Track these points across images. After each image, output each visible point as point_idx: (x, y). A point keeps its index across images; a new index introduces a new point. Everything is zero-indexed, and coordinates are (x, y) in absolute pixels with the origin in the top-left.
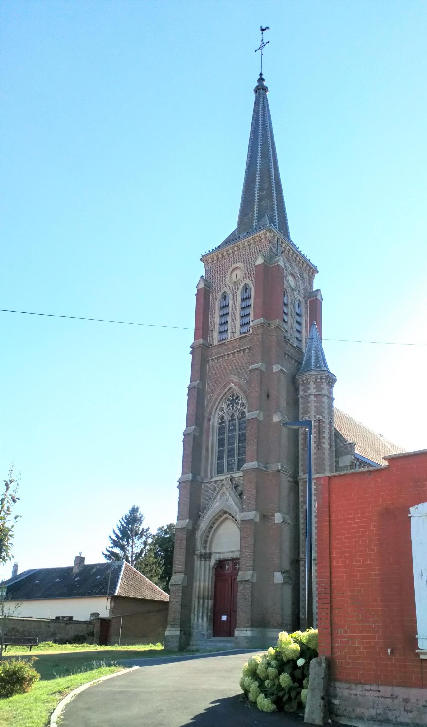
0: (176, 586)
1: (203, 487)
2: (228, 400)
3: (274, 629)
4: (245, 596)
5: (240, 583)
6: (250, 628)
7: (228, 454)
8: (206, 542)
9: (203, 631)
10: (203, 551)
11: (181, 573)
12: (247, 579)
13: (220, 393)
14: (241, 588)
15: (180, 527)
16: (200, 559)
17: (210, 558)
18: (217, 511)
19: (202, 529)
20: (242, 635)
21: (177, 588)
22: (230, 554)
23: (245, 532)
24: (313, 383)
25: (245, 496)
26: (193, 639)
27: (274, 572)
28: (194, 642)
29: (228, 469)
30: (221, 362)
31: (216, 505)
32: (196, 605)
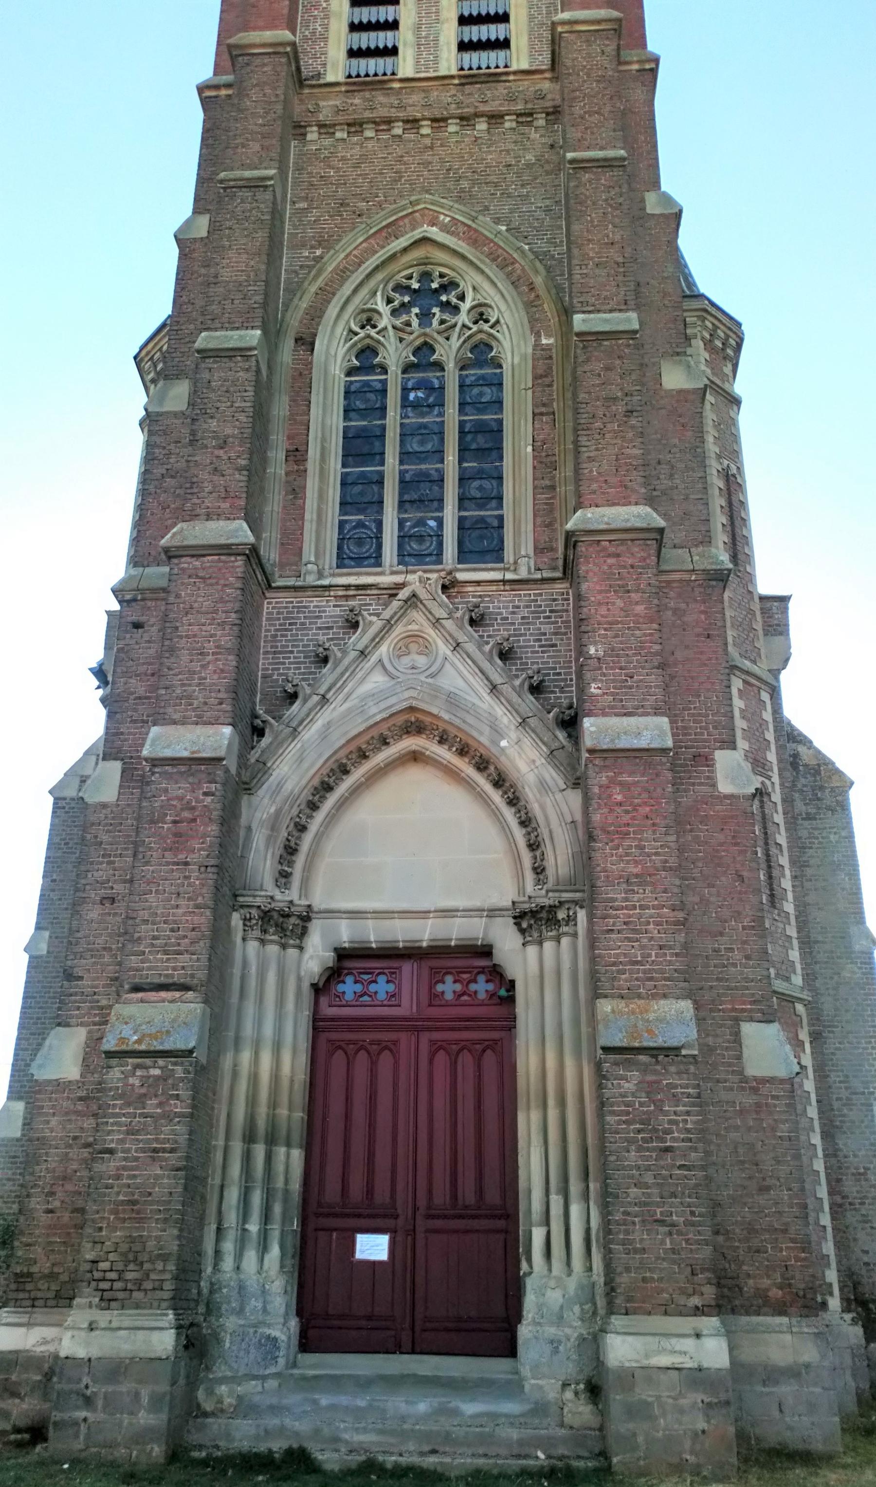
0: (148, 1061)
1: (266, 608)
2: (426, 276)
3: (769, 1320)
4: (657, 1134)
5: (616, 1064)
6: (712, 1322)
7: (401, 494)
8: (291, 850)
9: (269, 1326)
10: (281, 898)
11: (185, 988)
12: (674, 1043)
13: (366, 251)
14: (628, 1086)
15: (185, 754)
16: (257, 933)
17: (304, 932)
18: (376, 712)
19: (280, 786)
20: (665, 1360)
21: (157, 1072)
22: (458, 921)
23: (620, 804)
24: (701, 344)
25: (595, 643)
26: (221, 1370)
27: (737, 1020)
28: (223, 1389)
29: (401, 555)
30: (370, 145)
31: (367, 687)
32: (235, 1169)
